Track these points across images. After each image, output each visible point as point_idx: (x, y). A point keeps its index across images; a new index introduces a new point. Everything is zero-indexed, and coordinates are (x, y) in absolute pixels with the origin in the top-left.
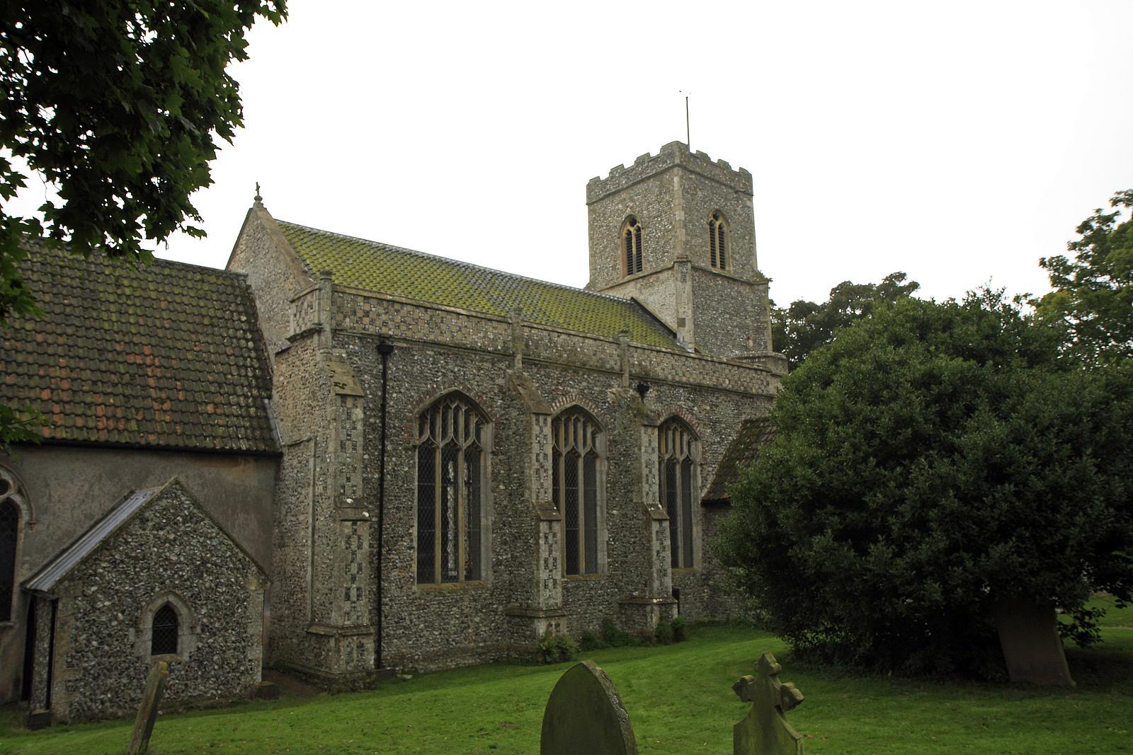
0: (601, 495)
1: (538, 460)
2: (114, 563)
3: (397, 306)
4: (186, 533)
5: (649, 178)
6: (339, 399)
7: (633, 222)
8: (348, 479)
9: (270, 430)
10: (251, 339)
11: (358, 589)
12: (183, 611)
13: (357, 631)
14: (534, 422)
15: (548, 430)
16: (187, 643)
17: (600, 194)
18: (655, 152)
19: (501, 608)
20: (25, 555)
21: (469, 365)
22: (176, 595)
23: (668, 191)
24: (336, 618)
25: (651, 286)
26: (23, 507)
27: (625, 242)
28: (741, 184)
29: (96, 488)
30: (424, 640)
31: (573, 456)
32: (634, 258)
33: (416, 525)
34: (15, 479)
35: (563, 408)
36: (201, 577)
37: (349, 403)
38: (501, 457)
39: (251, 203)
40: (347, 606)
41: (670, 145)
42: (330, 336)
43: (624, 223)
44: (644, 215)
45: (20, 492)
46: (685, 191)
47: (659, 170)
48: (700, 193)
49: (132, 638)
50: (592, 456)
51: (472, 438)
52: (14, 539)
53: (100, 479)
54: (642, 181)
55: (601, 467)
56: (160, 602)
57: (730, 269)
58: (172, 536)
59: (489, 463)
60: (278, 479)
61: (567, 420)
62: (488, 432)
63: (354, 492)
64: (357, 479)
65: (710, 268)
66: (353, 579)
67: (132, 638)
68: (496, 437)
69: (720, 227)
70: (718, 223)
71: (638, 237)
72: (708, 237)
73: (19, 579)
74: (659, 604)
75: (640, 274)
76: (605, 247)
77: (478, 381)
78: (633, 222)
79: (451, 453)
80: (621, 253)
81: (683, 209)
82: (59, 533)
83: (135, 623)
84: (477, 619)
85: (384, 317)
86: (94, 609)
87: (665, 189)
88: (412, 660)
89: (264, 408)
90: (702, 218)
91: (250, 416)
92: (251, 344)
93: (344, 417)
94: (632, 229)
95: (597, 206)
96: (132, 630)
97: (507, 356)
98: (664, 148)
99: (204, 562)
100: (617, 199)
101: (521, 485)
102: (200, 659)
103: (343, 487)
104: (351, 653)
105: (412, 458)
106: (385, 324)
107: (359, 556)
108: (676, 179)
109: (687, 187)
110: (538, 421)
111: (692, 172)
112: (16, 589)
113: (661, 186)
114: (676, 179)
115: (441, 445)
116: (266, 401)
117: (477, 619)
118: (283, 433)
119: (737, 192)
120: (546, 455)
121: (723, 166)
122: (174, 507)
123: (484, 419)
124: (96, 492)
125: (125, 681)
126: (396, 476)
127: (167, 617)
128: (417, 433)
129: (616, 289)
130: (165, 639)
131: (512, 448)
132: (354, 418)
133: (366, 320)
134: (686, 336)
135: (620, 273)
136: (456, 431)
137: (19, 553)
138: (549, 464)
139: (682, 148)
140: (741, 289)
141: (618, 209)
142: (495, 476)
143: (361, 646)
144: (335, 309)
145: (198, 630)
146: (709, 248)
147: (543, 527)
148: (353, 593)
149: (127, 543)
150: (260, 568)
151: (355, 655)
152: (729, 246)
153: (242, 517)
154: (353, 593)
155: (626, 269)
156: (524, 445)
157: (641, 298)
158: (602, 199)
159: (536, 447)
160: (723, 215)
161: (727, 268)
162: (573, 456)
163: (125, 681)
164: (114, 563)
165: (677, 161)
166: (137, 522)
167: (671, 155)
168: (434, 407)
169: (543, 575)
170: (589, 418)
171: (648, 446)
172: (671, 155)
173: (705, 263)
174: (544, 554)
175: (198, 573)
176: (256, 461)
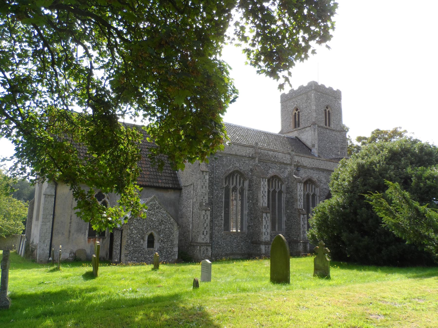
0: (283, 205)
6: (201, 172)
7: (297, 110)
8: (204, 197)
11: (207, 232)
12: (156, 235)
13: (206, 244)
15: (266, 183)
16: (157, 245)
19: (249, 241)
22: (154, 230)
24: (199, 240)
25: (303, 132)
26: (109, 203)
31: (274, 191)
36: (161, 226)
37: (205, 174)
43: (293, 110)
45: (108, 198)
46: (316, 99)
49: (142, 242)
50: (280, 192)
55: (284, 196)
56: (149, 232)
57: (332, 126)
58: (153, 213)
59: (247, 193)
60: (180, 196)
66: (205, 228)
67: (142, 242)
69: (329, 111)
70: (327, 110)
72: (324, 115)
74: (303, 243)
78: (297, 110)
79: (235, 189)
80: (292, 120)
83: (143, 238)
86: (132, 233)
89: (176, 174)
93: (203, 178)
94: (296, 112)
97: (253, 158)
98: (309, 84)
99: (162, 221)
101: (257, 201)
103: (202, 200)
105: (223, 191)
110: (263, 180)
113: (307, 97)
118: (183, 182)
120: (265, 192)
121: (331, 89)
123: (245, 179)
125: (140, 255)
126: (217, 197)
127: (151, 237)
130: (151, 243)
134: (315, 151)
138: (266, 194)
141: (292, 106)
143: (207, 249)
145: (160, 241)
146: (324, 119)
147: (264, 215)
148: (205, 233)
154: (205, 233)
155: (294, 126)
156: (258, 188)
157: (299, 137)
160: (330, 107)
162: (274, 191)
163: (140, 255)
168: (230, 174)
169: (264, 230)
170: (280, 179)
171: (300, 190)
173: (323, 124)
174: (264, 223)
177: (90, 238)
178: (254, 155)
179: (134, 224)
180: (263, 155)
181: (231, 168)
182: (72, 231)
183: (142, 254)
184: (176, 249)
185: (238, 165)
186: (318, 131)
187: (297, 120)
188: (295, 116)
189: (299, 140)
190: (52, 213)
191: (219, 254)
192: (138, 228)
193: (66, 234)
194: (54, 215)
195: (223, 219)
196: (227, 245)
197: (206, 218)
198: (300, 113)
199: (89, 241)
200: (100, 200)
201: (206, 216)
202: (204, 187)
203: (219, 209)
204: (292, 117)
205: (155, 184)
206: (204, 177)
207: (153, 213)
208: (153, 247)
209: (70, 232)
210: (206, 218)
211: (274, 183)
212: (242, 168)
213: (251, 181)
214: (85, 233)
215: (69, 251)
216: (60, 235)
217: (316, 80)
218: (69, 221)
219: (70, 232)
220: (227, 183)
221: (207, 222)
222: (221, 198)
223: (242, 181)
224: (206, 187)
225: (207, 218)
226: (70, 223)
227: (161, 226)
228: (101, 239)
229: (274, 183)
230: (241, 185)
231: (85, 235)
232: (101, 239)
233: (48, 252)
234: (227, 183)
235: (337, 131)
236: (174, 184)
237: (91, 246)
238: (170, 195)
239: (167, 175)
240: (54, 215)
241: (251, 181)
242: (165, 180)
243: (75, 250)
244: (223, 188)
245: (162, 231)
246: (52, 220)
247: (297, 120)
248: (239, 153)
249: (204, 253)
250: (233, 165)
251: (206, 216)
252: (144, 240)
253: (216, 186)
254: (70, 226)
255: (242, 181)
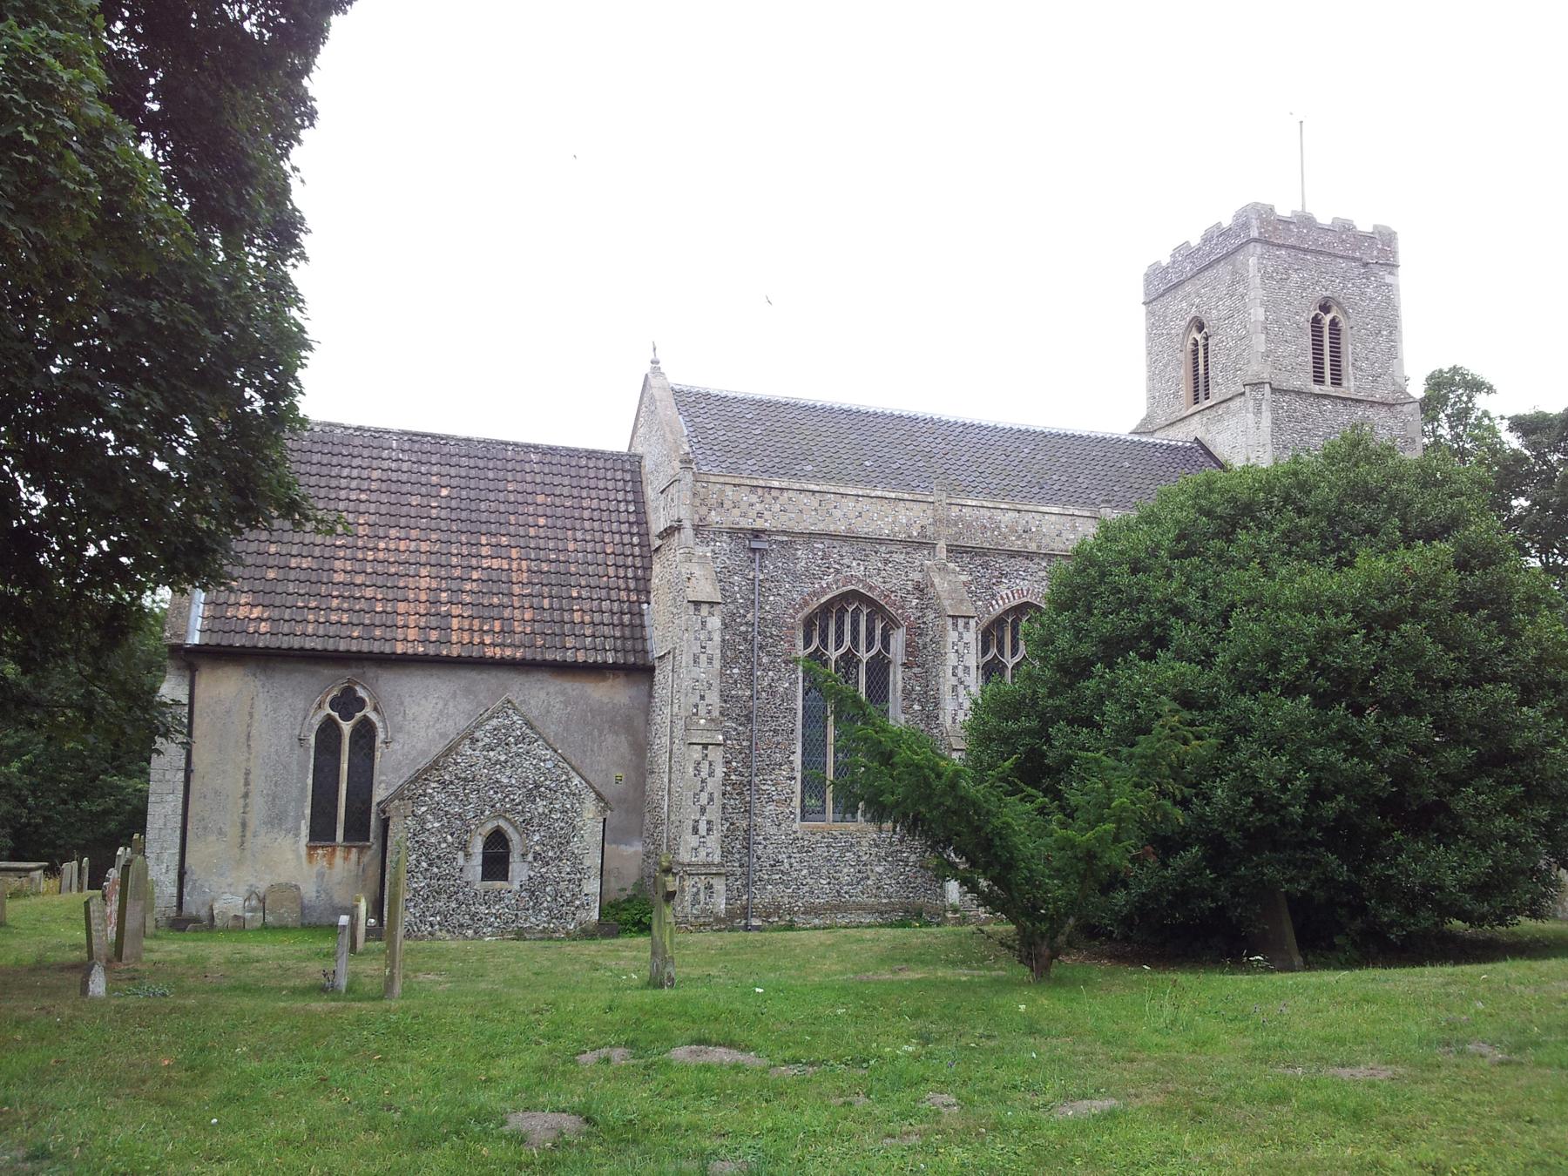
1: (954, 674)
2: (443, 783)
3: (775, 493)
4: (518, 755)
5: (1218, 261)
6: (692, 607)
7: (1200, 328)
8: (702, 698)
9: (644, 639)
10: (638, 534)
11: (709, 822)
14: (950, 627)
16: (519, 871)
17: (1163, 286)
18: (1227, 222)
19: (913, 858)
20: (382, 773)
21: (873, 557)
22: (507, 819)
23: (1243, 280)
24: (685, 856)
25: (1220, 419)
26: (379, 725)
27: (1190, 357)
28: (1372, 254)
29: (451, 704)
30: (806, 888)
32: (1201, 380)
33: (799, 750)
34: (371, 696)
35: (1007, 606)
36: (534, 802)
37: (705, 610)
38: (916, 670)
39: (647, 368)
40: (694, 841)
41: (1244, 210)
42: (691, 533)
43: (1188, 329)
44: (1211, 320)
45: (375, 709)
46: (1266, 277)
47: (1231, 248)
48: (1294, 276)
49: (461, 862)
51: (877, 646)
52: (372, 759)
53: (454, 696)
54: (1210, 265)
56: (490, 826)
57: (1350, 386)
58: (503, 758)
59: (899, 677)
60: (651, 696)
61: (842, 612)
62: (898, 640)
63: (709, 712)
64: (713, 698)
65: (1317, 389)
66: (703, 810)
67: (461, 862)
68: (908, 646)
69: (1333, 323)
70: (1327, 319)
71: (1206, 347)
72: (1307, 341)
73: (376, 799)
75: (1208, 403)
76: (1166, 366)
77: (880, 577)
78: (1200, 328)
80: (1184, 373)
81: (1262, 304)
82: (414, 753)
83: (464, 847)
84: (880, 869)
85: (758, 507)
86: (424, 830)
87: (1238, 278)
88: (790, 911)
90: (1297, 313)
91: (622, 624)
92: (635, 540)
93: (698, 626)
94: (1199, 337)
95: (1157, 305)
96: (461, 854)
97: (922, 544)
98: (1237, 216)
99: (537, 787)
100: (1180, 293)
102: (532, 890)
103: (696, 706)
104: (697, 893)
105: (794, 671)
106: (760, 515)
107: (710, 784)
108: (1252, 261)
109: (1270, 269)
110: (955, 625)
111: (1280, 246)
112: (374, 809)
113: (1234, 272)
114: (1252, 261)
115: (833, 658)
116: (645, 606)
117: (880, 869)
119: (1366, 265)
120: (967, 669)
121: (1344, 230)
122: (504, 726)
123: (891, 623)
124: (451, 710)
125: (453, 905)
126: (774, 694)
128: (800, 643)
129: (1179, 425)
130: (496, 862)
131: (921, 656)
132: (709, 626)
133: (736, 512)
135: (1184, 407)
136: (855, 639)
137: (376, 772)
139: (1265, 215)
140: (1370, 412)
141: (1181, 308)
142: (907, 694)
143: (709, 887)
144: (697, 502)
145: (530, 858)
146: (1310, 358)
148: (703, 827)
149: (456, 764)
150: (598, 795)
151: (702, 896)
152: (1348, 349)
153: (610, 739)
154: (703, 827)
155: (1191, 394)
157: (1207, 439)
158: (1162, 295)
159: (952, 659)
160: (1338, 304)
161: (1345, 383)
163: (453, 905)
164: (443, 783)
165: (1254, 234)
166: (467, 741)
167: (1246, 226)
168: (825, 609)
172: (1246, 226)
173: (1305, 381)
175: (530, 796)
176: (626, 675)
177: (316, 848)
178: (930, 531)
179: (432, 797)
180: (969, 526)
181: (830, 587)
182: (254, 822)
183: (460, 904)
184: (592, 886)
185: (859, 571)
186: (1274, 411)
187: (1201, 371)
188: (1195, 352)
189: (1209, 454)
190: (183, 764)
191: (779, 907)
192: (447, 813)
193: (233, 832)
194: (188, 771)
195: (799, 776)
196: (814, 872)
197: (704, 774)
198: (1210, 341)
199: (310, 856)
200: (347, 717)
201: (705, 767)
202: (703, 658)
203: (779, 738)
204: (1185, 357)
205: (549, 656)
206: (704, 623)
207: (503, 758)
208: (504, 876)
209: (244, 825)
210: (704, 774)
211: (847, 628)
212: (876, 581)
213: (916, 631)
214: (298, 828)
215: (243, 889)
216: (212, 838)
217: (1265, 199)
218: (243, 790)
219: (244, 825)
220: (816, 643)
221: (709, 789)
222: (788, 697)
223: (878, 632)
224: (710, 660)
225: (711, 774)
226: (246, 795)
227: (534, 802)
228: (354, 853)
229: (847, 628)
230: (877, 646)
231: (297, 835)
232: (354, 853)
233: (174, 891)
234: (816, 643)
235: (1372, 404)
236: (625, 651)
237: (321, 875)
238: (611, 694)
239: (606, 618)
240: (188, 771)
241: (916, 631)
242: (593, 636)
243: (262, 887)
244: (796, 661)
245: (536, 821)
246: (181, 788)
247: (1201, 371)
248: (862, 528)
249: (695, 902)
250: (837, 571)
251: (705, 767)
252: (467, 855)
253: (768, 654)
254: (246, 805)
255: (878, 632)
